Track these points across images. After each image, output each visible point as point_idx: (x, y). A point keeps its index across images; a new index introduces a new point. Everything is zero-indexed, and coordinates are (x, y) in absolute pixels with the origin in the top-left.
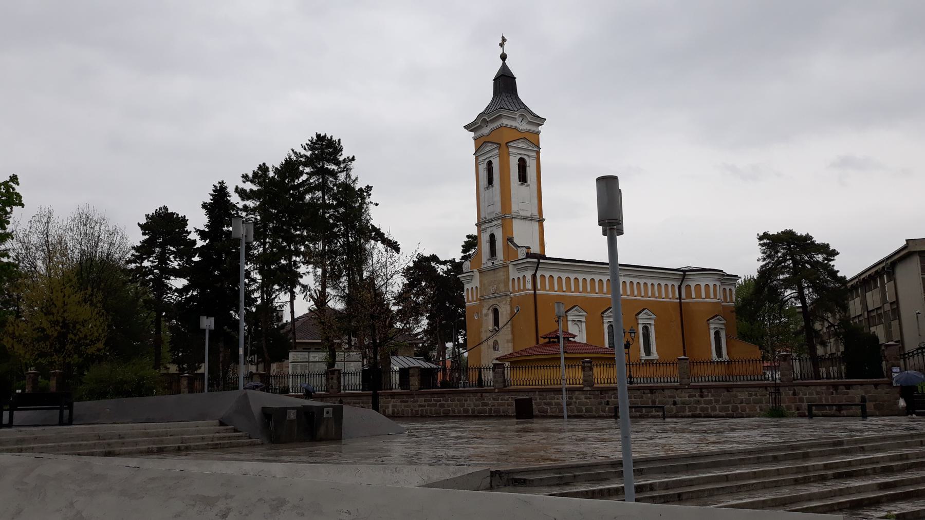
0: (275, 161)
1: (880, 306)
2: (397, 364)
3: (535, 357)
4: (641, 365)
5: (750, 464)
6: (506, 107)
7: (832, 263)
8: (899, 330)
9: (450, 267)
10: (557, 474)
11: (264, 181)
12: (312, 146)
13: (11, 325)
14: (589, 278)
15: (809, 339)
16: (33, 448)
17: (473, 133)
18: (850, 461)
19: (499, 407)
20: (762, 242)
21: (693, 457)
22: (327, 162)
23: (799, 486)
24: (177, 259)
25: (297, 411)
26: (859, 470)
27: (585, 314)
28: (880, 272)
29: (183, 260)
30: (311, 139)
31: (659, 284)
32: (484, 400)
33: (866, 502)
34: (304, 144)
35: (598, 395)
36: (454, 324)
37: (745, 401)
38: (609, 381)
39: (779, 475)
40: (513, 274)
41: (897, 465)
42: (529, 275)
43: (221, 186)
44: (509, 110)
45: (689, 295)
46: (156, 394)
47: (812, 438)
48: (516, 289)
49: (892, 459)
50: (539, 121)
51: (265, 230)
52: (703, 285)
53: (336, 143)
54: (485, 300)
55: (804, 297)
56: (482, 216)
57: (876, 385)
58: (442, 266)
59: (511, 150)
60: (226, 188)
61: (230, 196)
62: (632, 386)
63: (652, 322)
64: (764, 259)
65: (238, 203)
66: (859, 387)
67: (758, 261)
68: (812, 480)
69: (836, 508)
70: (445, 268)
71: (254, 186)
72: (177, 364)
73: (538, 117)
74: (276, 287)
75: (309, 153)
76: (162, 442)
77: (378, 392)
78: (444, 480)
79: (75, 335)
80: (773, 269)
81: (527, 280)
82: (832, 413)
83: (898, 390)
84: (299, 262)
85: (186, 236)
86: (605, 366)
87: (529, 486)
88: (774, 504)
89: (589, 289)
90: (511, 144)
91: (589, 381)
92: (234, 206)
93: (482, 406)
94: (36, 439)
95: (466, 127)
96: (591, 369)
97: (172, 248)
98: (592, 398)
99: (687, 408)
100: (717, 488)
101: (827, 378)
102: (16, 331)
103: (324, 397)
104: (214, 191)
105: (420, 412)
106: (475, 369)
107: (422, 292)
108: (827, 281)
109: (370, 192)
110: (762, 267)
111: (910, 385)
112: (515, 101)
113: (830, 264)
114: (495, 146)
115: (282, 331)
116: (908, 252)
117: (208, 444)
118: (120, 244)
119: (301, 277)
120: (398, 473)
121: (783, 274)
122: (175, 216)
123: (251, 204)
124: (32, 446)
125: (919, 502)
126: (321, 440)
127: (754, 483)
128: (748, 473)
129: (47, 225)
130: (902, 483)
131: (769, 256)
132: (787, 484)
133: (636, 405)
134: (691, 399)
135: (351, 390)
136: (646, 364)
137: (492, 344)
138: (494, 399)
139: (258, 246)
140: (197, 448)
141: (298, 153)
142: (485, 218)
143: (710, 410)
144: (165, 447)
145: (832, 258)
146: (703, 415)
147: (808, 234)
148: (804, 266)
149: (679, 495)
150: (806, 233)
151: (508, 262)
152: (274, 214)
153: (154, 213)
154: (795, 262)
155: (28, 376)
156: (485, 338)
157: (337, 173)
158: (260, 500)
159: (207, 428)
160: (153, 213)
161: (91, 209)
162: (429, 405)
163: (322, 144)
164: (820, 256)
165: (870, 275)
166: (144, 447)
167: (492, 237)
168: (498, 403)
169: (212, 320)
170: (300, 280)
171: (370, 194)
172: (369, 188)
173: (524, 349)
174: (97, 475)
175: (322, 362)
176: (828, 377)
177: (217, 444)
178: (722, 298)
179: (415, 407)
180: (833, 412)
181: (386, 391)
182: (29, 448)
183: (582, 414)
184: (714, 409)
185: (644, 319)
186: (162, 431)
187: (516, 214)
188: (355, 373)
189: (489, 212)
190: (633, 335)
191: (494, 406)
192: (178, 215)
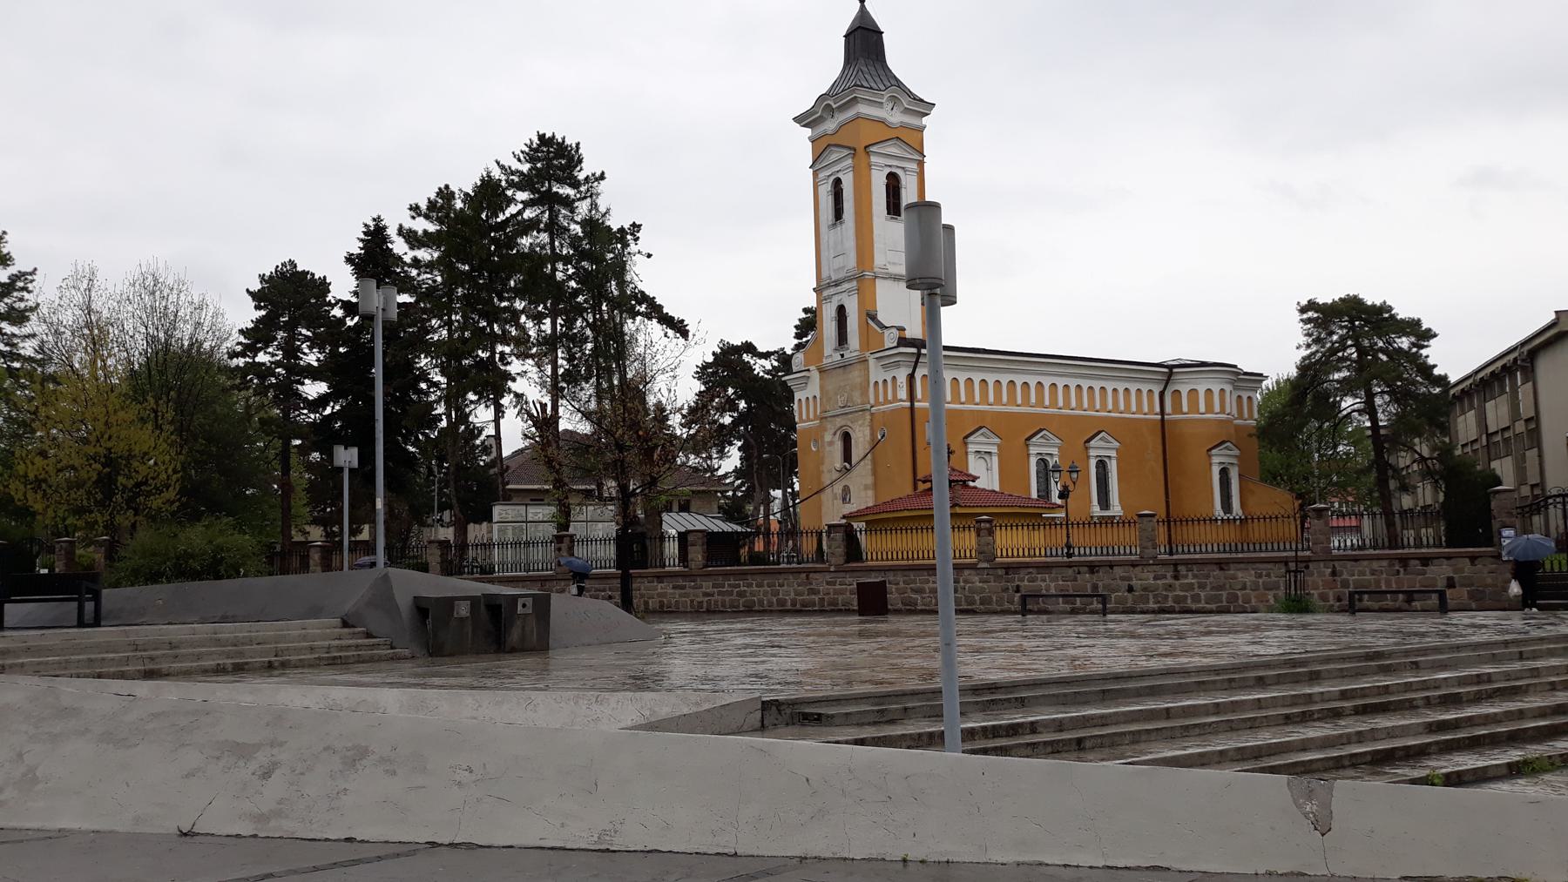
0: (465, 182)
1: (1508, 425)
2: (673, 524)
3: (906, 514)
4: (1092, 526)
5: (1217, 690)
6: (865, 84)
7: (1424, 352)
8: (1537, 466)
9: (776, 364)
10: (877, 705)
11: (447, 216)
12: (532, 155)
13: (21, 463)
14: (1005, 379)
15: (1382, 482)
16: (22, 665)
17: (810, 130)
18: (1387, 685)
19: (836, 596)
20: (1305, 316)
21: (1118, 677)
22: (558, 183)
23: (1291, 727)
24: (314, 350)
25: (471, 604)
26: (1400, 701)
27: (997, 440)
28: (1510, 367)
29: (324, 352)
30: (528, 142)
31: (1222, 390)
32: (811, 584)
33: (1401, 753)
34: (518, 152)
35: (1002, 576)
36: (784, 458)
37: (1250, 586)
38: (1032, 553)
39: (1260, 708)
40: (876, 373)
41: (1469, 692)
42: (902, 375)
43: (377, 224)
44: (862, 86)
45: (1177, 407)
46: (245, 575)
47: (1334, 647)
48: (881, 399)
49: (1462, 681)
50: (923, 107)
51: (451, 301)
52: (1202, 390)
53: (571, 150)
54: (829, 419)
55: (1375, 410)
56: (825, 275)
57: (1473, 559)
58: (763, 362)
59: (873, 159)
60: (385, 228)
61: (392, 243)
62: (1070, 560)
63: (1113, 454)
64: (1308, 346)
65: (406, 253)
66: (1445, 562)
67: (1297, 348)
68: (1316, 716)
69: (1347, 763)
70: (767, 364)
71: (431, 224)
72: (322, 525)
73: (922, 100)
74: (471, 396)
75: (525, 168)
76: (241, 654)
77: (631, 571)
78: (679, 717)
79: (129, 477)
80: (1323, 362)
81: (898, 384)
82: (1397, 606)
83: (1509, 566)
84: (510, 355)
85: (329, 312)
86: (1025, 528)
87: (826, 726)
88: (1240, 757)
89: (1005, 399)
90: (873, 149)
91: (987, 554)
92: (400, 258)
93: (808, 595)
94: (28, 651)
95: (797, 120)
96: (991, 532)
97: (304, 331)
98: (992, 580)
99: (1151, 597)
100: (1147, 730)
101: (1416, 547)
102: (29, 471)
103: (546, 580)
104: (365, 233)
105: (705, 605)
106: (812, 532)
107: (730, 405)
108: (1414, 383)
109: (638, 235)
110: (1304, 359)
111: (1531, 559)
112: (881, 72)
113: (1421, 355)
114: (846, 152)
115: (492, 471)
116: (1559, 332)
117: (319, 658)
118: (213, 324)
119: (514, 380)
120: (601, 704)
121: (1339, 370)
122: (309, 277)
123: (424, 255)
124: (21, 661)
125: (1491, 752)
126: (513, 650)
127: (1213, 722)
128: (1205, 705)
129: (87, 293)
130: (1470, 722)
131: (1317, 341)
132: (1272, 724)
133: (1067, 593)
134: (1158, 582)
135: (601, 568)
136: (1101, 523)
137: (840, 491)
138: (828, 583)
139: (440, 327)
140: (301, 665)
141: (507, 167)
142: (830, 278)
143: (1189, 601)
144: (247, 663)
145: (1426, 343)
146: (1177, 609)
147: (1385, 302)
148: (1376, 358)
149: (1079, 741)
150: (1382, 301)
151: (867, 354)
152: (463, 272)
153: (274, 271)
154: (1362, 351)
155: (57, 546)
156: (829, 482)
157: (574, 201)
158: (326, 749)
159: (321, 631)
160: (272, 273)
161: (162, 265)
162: (720, 593)
163: (549, 152)
164: (1404, 339)
165: (1493, 373)
166: (212, 663)
167: (841, 310)
168: (834, 589)
169: (355, 451)
170: (510, 383)
171: (638, 238)
172: (636, 227)
173: (889, 500)
174: (66, 709)
175: (549, 522)
176: (1419, 544)
177: (335, 658)
178: (1235, 412)
179: (697, 597)
180: (1397, 604)
181: (655, 571)
182: (16, 665)
183: (974, 607)
184: (1196, 598)
185: (1098, 449)
186: (244, 637)
187: (883, 271)
188: (604, 540)
189: (835, 268)
190: (1075, 475)
191: (829, 594)
192: (313, 275)
